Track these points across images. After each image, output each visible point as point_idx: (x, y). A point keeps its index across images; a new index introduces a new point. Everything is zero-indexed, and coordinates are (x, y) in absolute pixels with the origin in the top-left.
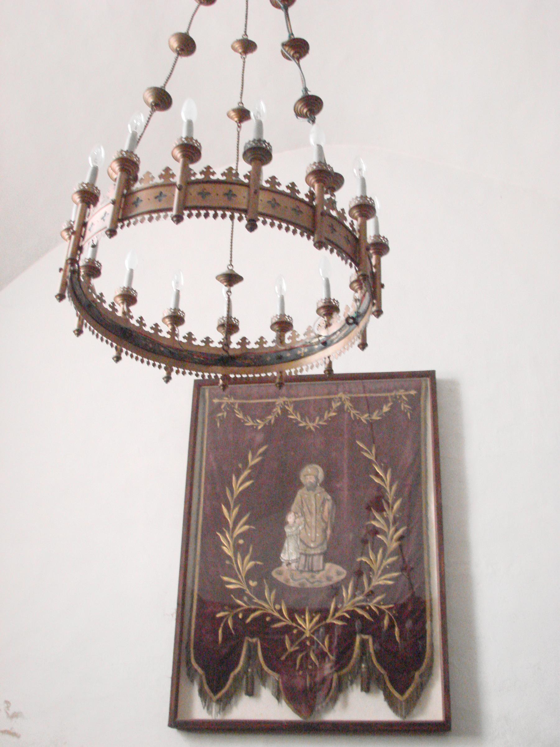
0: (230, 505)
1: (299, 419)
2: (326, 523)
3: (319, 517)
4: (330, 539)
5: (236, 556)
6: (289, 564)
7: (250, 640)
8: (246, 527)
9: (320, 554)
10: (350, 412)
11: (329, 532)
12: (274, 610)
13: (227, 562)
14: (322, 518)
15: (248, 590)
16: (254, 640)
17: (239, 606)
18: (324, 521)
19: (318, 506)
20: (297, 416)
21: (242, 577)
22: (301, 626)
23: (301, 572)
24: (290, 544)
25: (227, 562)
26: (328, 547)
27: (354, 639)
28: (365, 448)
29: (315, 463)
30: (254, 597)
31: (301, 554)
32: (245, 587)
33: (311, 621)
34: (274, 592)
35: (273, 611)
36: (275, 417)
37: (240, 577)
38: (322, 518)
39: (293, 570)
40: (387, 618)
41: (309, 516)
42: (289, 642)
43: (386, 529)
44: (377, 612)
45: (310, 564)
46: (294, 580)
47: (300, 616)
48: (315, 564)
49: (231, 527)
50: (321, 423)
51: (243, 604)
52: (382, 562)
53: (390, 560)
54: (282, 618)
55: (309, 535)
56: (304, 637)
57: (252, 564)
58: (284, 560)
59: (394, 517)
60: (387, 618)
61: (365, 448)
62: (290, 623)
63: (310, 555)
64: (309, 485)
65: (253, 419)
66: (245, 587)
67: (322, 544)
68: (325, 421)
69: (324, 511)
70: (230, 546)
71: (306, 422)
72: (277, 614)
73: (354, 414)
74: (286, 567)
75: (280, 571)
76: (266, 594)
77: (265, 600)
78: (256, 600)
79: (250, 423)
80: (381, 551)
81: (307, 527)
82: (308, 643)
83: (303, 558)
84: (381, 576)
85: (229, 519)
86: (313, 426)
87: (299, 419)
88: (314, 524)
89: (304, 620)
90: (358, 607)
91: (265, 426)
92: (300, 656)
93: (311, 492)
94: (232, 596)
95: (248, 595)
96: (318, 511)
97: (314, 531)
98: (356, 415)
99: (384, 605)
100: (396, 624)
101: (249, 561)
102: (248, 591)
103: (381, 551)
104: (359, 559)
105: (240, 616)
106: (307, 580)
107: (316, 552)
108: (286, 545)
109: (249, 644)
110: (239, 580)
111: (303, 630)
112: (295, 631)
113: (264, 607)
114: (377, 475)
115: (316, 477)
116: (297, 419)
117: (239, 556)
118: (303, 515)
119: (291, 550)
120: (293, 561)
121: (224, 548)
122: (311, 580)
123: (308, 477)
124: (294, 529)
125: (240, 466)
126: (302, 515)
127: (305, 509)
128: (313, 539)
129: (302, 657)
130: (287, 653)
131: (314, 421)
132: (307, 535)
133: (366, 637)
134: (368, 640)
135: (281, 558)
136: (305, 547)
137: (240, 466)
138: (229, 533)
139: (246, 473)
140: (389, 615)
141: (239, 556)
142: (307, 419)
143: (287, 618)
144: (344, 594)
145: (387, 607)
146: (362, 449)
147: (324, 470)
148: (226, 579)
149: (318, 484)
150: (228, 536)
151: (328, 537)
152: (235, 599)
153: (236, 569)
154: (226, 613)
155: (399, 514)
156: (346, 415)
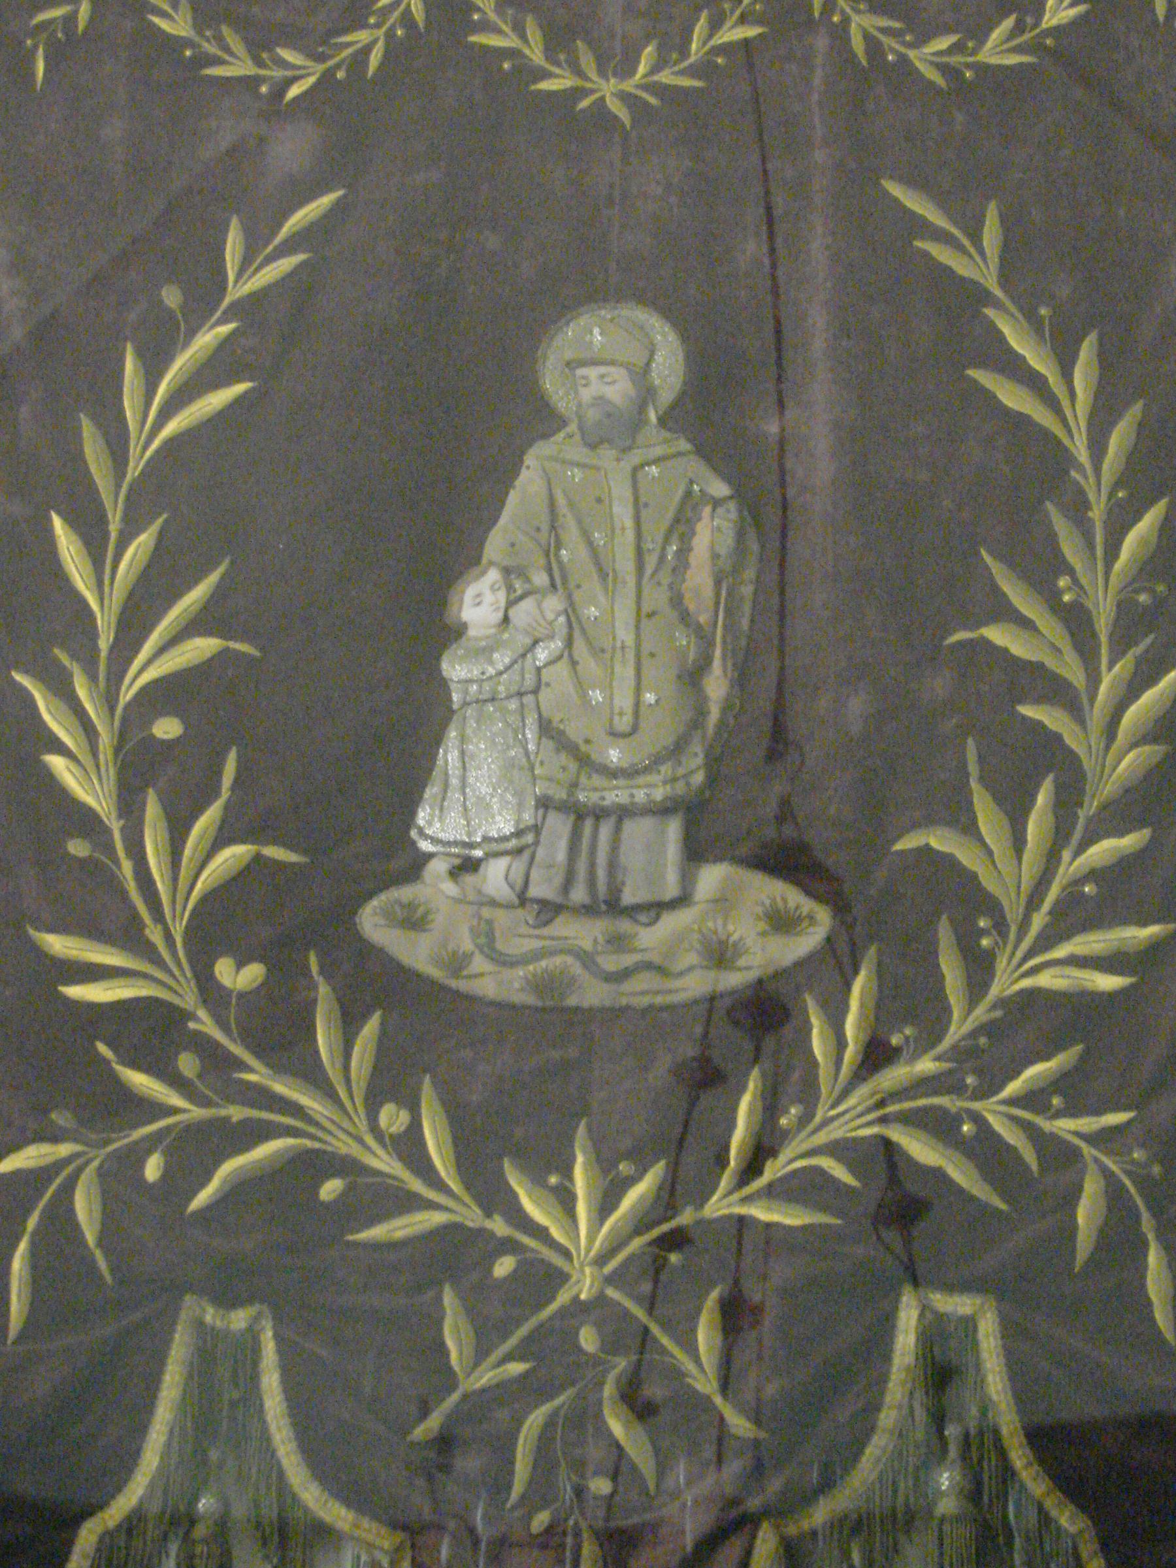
0: (102, 520)
1: (536, 55)
2: (705, 640)
3: (657, 598)
4: (722, 725)
5: (130, 807)
6: (467, 866)
7: (210, 1315)
8: (203, 647)
9: (664, 810)
10: (846, 21)
11: (716, 686)
12: (369, 1140)
13: (78, 848)
14: (677, 601)
15: (202, 1013)
16: (239, 1319)
17: (155, 1110)
18: (685, 617)
19: (655, 532)
20: (523, 37)
21: (168, 937)
22: (541, 1233)
23: (549, 910)
24: (478, 746)
25: (78, 848)
26: (712, 780)
27: (887, 1324)
28: (937, 219)
29: (641, 298)
30: (237, 1050)
31: (544, 803)
32: (188, 998)
33: (605, 1205)
34: (371, 1028)
35: (360, 1141)
36: (390, 35)
37: (154, 934)
38: (677, 601)
39: (493, 903)
40: (1092, 1189)
41: (598, 588)
42: (468, 1335)
43: (1072, 670)
44: (1030, 1157)
45: (601, 873)
46: (505, 962)
47: (537, 1179)
48: (633, 857)
49: (104, 644)
50: (665, 77)
51: (176, 1100)
52: (1052, 858)
53: (1104, 850)
54: (416, 1185)
55: (597, 696)
56: (563, 1298)
57: (234, 854)
58: (435, 840)
59: (1124, 607)
60: (1092, 1189)
61: (937, 219)
62: (472, 1216)
63: (599, 814)
64: (592, 415)
65: (258, 47)
66: (188, 998)
67: (677, 750)
68: (691, 72)
69: (687, 566)
70: (95, 753)
71: (580, 73)
72: (383, 1162)
73: (867, 37)
74: (450, 888)
75: (411, 906)
76: (324, 1039)
77: (313, 1076)
78: (257, 1074)
79: (239, 67)
80: (1043, 798)
81: (579, 644)
82: (588, 1339)
83: (558, 826)
84: (1046, 941)
85: (94, 605)
86: (624, 97)
87: (536, 55)
88: (626, 635)
89: (565, 1200)
90: (908, 1119)
91: (327, 77)
92: (535, 1419)
93: (607, 455)
94: (102, 1048)
95: (204, 1047)
96: (651, 562)
97: (625, 672)
98: (885, 40)
99: (1071, 1111)
100: (1147, 1224)
101: (221, 839)
102: (205, 1023)
103: (1043, 798)
104: (908, 843)
105: (153, 1169)
106: (587, 959)
107: (640, 796)
108: (449, 756)
109: (205, 1336)
110: (148, 952)
111: (558, 1261)
112: (504, 1267)
113: (297, 1110)
114: (1014, 368)
115: (641, 375)
116: (527, 52)
117: (152, 810)
118: (559, 581)
119: (482, 781)
120: (497, 848)
121: (56, 762)
122: (611, 963)
123: (592, 372)
124: (502, 659)
125: (172, 297)
126: (553, 585)
127: (572, 553)
128: (624, 723)
129: (550, 1423)
130: (455, 1397)
131: (627, 68)
132: (584, 695)
133: (959, 1305)
134: (969, 1324)
135: (413, 834)
136: (573, 766)
137: (172, 297)
138: (93, 677)
139: (207, 339)
140: (1107, 1174)
141: (152, 810)
142: (588, 62)
143: (454, 1185)
144: (818, 1045)
145: (1088, 1124)
146: (922, 227)
147: (685, 338)
148: (58, 944)
149: (653, 417)
150: (82, 693)
151: (715, 713)
152: (118, 1068)
153: (132, 887)
154: (64, 1149)
155: (1152, 591)
156: (821, 43)
